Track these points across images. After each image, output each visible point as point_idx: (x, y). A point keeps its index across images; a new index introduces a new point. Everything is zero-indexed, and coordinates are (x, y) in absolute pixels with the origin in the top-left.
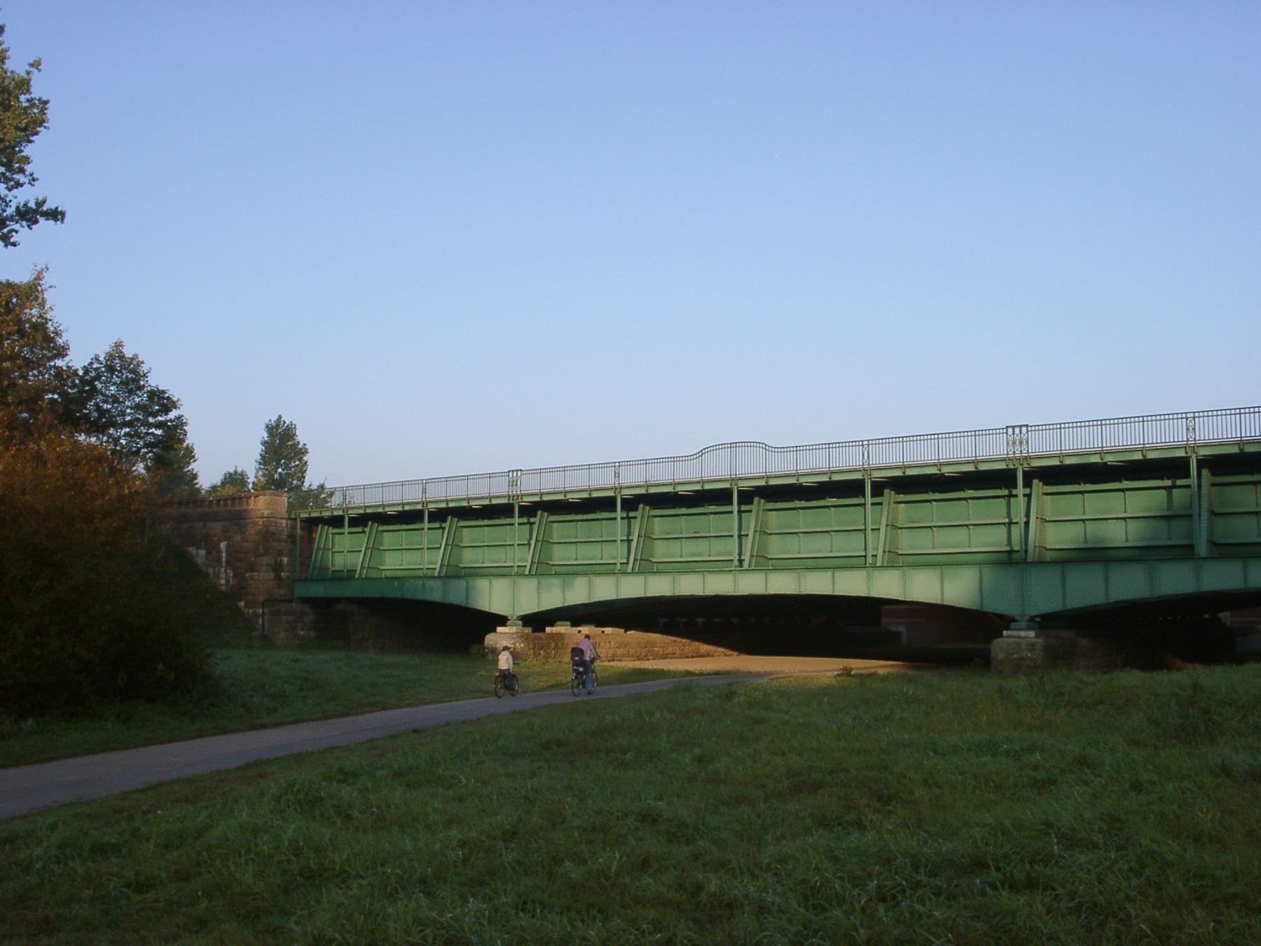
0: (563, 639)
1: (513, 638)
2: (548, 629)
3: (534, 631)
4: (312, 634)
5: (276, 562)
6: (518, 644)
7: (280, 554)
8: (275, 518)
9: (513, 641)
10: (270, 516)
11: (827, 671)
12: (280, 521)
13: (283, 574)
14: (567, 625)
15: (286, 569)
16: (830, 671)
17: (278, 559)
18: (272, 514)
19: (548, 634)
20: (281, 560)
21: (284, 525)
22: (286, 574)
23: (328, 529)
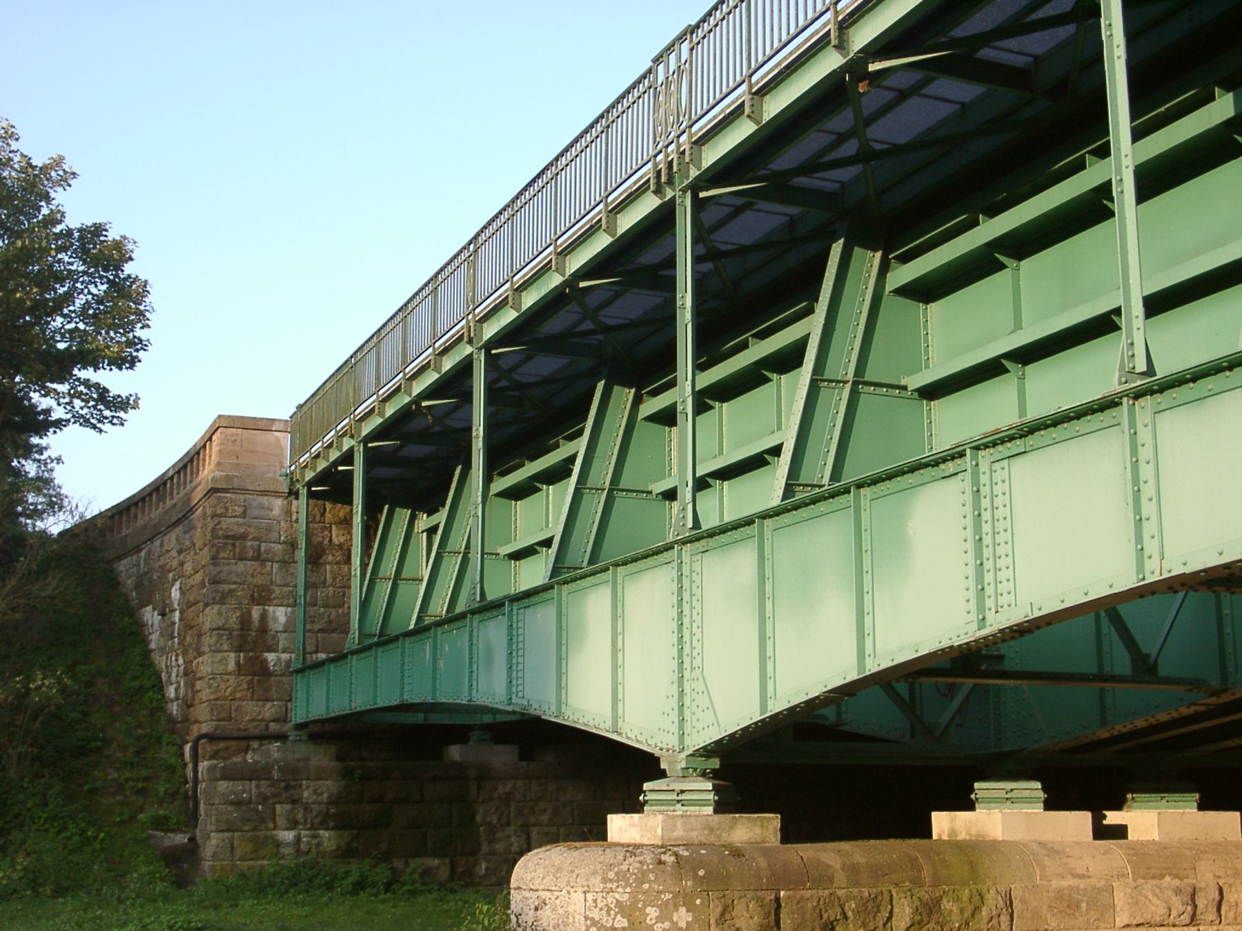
0: (974, 872)
1: (622, 877)
2: (942, 822)
3: (788, 836)
4: (327, 837)
5: (245, 621)
6: (652, 912)
7: (262, 596)
8: (244, 491)
9: (622, 895)
10: (223, 485)
11: (478, 666)
12: (264, 500)
13: (271, 657)
14: (1030, 800)
15: (283, 641)
16: (478, 669)
17: (256, 612)
18: (228, 478)
19: (1131, 841)
20: (264, 617)
21: (276, 512)
22: (285, 656)
23: (413, 518)
